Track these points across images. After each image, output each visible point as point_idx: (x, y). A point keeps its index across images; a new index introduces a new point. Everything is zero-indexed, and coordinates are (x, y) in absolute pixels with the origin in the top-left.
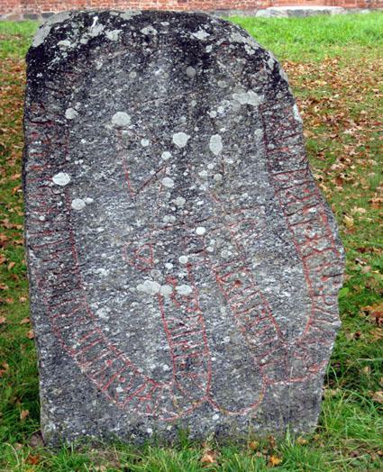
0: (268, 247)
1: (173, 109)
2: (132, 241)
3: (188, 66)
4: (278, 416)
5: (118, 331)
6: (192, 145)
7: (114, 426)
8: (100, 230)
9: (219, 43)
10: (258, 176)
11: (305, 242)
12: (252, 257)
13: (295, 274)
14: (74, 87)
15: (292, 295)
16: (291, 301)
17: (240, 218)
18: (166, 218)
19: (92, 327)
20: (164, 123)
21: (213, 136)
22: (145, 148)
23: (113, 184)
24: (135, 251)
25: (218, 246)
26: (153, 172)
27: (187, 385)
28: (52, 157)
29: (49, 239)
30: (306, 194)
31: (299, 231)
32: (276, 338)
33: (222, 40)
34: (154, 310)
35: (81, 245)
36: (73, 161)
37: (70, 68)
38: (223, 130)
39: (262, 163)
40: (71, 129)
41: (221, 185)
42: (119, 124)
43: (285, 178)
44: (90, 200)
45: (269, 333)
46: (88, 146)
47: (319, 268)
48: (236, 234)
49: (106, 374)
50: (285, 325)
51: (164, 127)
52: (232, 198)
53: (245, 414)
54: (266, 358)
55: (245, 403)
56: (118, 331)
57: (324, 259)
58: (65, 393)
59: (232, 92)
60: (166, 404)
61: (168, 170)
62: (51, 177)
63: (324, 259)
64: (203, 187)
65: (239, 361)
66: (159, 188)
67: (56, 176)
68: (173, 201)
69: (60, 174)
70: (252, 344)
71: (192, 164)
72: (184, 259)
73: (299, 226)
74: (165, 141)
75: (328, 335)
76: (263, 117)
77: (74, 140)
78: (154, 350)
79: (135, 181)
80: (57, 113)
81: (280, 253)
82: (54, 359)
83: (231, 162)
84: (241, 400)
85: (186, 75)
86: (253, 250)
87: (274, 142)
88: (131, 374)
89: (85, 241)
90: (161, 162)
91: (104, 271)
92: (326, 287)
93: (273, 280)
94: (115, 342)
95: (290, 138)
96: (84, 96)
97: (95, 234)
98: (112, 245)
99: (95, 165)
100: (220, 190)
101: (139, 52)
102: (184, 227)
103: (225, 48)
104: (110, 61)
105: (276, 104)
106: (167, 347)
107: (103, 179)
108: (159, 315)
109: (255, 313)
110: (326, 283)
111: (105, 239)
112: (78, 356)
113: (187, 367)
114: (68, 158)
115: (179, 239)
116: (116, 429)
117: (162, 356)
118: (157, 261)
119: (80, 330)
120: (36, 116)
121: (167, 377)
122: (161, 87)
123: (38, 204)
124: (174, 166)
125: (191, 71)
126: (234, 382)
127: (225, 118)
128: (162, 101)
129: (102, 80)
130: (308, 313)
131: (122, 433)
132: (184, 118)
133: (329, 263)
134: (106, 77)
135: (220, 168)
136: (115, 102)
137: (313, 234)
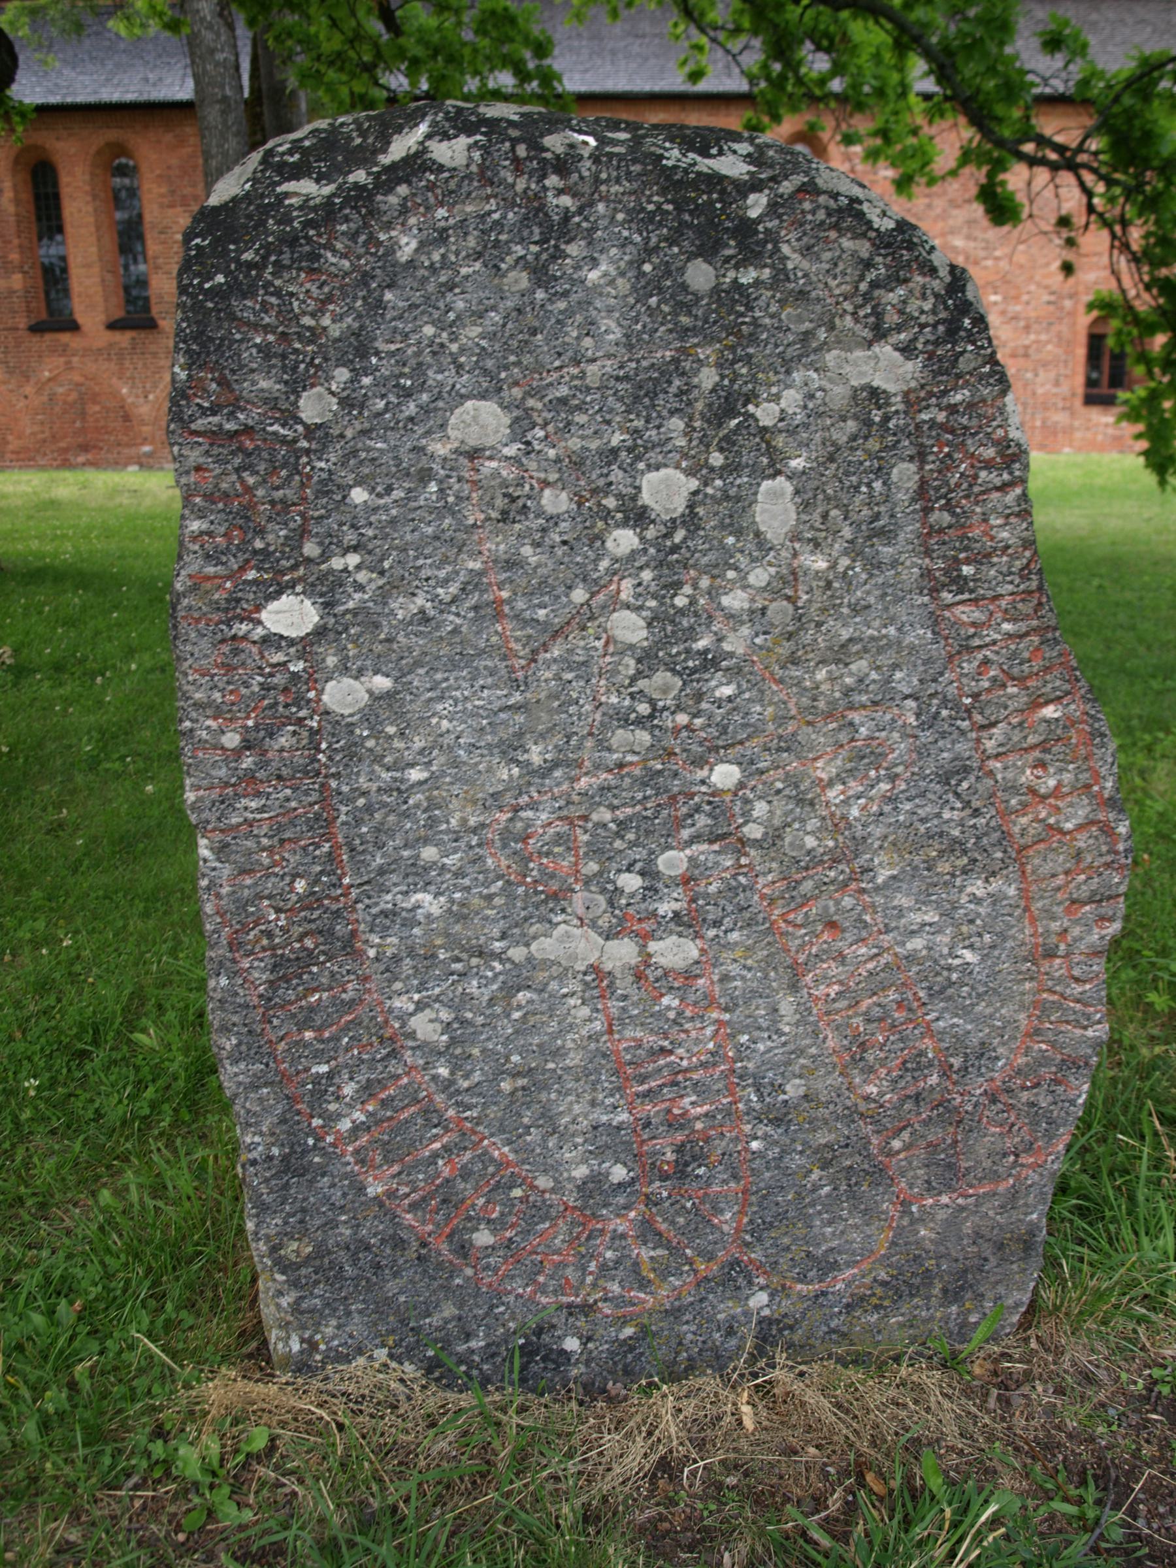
0: (923, 820)
1: (645, 392)
2: (516, 809)
3: (691, 256)
4: (931, 1285)
5: (477, 1077)
6: (700, 511)
7: (468, 1336)
8: (415, 775)
9: (786, 187)
10: (900, 610)
11: (1024, 805)
12: (875, 852)
13: (996, 899)
14: (326, 321)
15: (984, 958)
16: (980, 973)
17: (843, 737)
18: (620, 736)
19: (394, 1067)
20: (616, 439)
21: (766, 485)
22: (554, 520)
23: (456, 631)
24: (525, 839)
25: (777, 822)
26: (579, 595)
27: (681, 1220)
28: (259, 544)
29: (253, 805)
30: (1037, 665)
31: (1010, 775)
32: (934, 1079)
33: (799, 179)
34: (585, 1011)
35: (359, 822)
36: (325, 557)
37: (314, 257)
38: (797, 463)
39: (910, 574)
40: (320, 453)
41: (790, 636)
42: (472, 442)
43: (978, 615)
44: (382, 683)
45: (915, 1065)
46: (375, 510)
47: (1060, 880)
48: (831, 784)
49: (447, 1197)
50: (960, 1040)
51: (615, 452)
52: (821, 675)
53: (840, 1286)
54: (905, 1135)
55: (842, 1259)
56: (477, 1077)
57: (1078, 855)
58: (321, 1251)
59: (824, 346)
60: (620, 1273)
61: (627, 591)
62: (258, 608)
63: (1078, 855)
64: (736, 644)
65: (828, 1146)
66: (599, 644)
67: (273, 606)
68: (642, 684)
69: (286, 600)
70: (867, 1098)
71: (702, 572)
72: (672, 861)
73: (1011, 758)
74: (619, 496)
75: (1071, 1064)
76: (918, 427)
77: (332, 489)
78: (585, 1124)
79: (526, 623)
80: (271, 402)
81: (955, 841)
82: (285, 1158)
83: (822, 565)
84: (832, 1249)
85: (684, 287)
86: (879, 831)
87: (949, 507)
88: (517, 1193)
89: (369, 809)
90: (604, 564)
91: (428, 903)
92: (1076, 931)
93: (932, 917)
94: (469, 1107)
95: (995, 495)
96: (358, 349)
97: (401, 790)
98: (454, 822)
99: (398, 572)
100: (785, 649)
101: (536, 208)
102: (677, 764)
103: (807, 206)
104: (442, 237)
105: (955, 388)
106: (624, 1117)
107: (423, 617)
108: (598, 1026)
109: (877, 1012)
110: (1076, 922)
111: (432, 804)
112: (357, 1152)
113: (681, 1171)
114: (310, 549)
115: (663, 802)
116: (473, 1344)
117: (606, 1141)
118: (593, 867)
119: (362, 1078)
120: (204, 412)
121: (621, 1200)
122: (606, 323)
123: (217, 696)
124: (647, 575)
125: (700, 275)
126: (812, 1204)
127: (806, 426)
128: (609, 366)
129: (417, 298)
130: (1023, 1007)
131: (493, 1355)
132: (677, 424)
133: (1090, 867)
134: (431, 287)
135: (789, 580)
136: (459, 367)
137: (1052, 783)
